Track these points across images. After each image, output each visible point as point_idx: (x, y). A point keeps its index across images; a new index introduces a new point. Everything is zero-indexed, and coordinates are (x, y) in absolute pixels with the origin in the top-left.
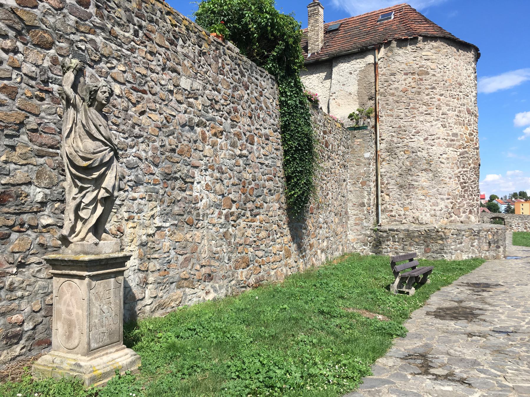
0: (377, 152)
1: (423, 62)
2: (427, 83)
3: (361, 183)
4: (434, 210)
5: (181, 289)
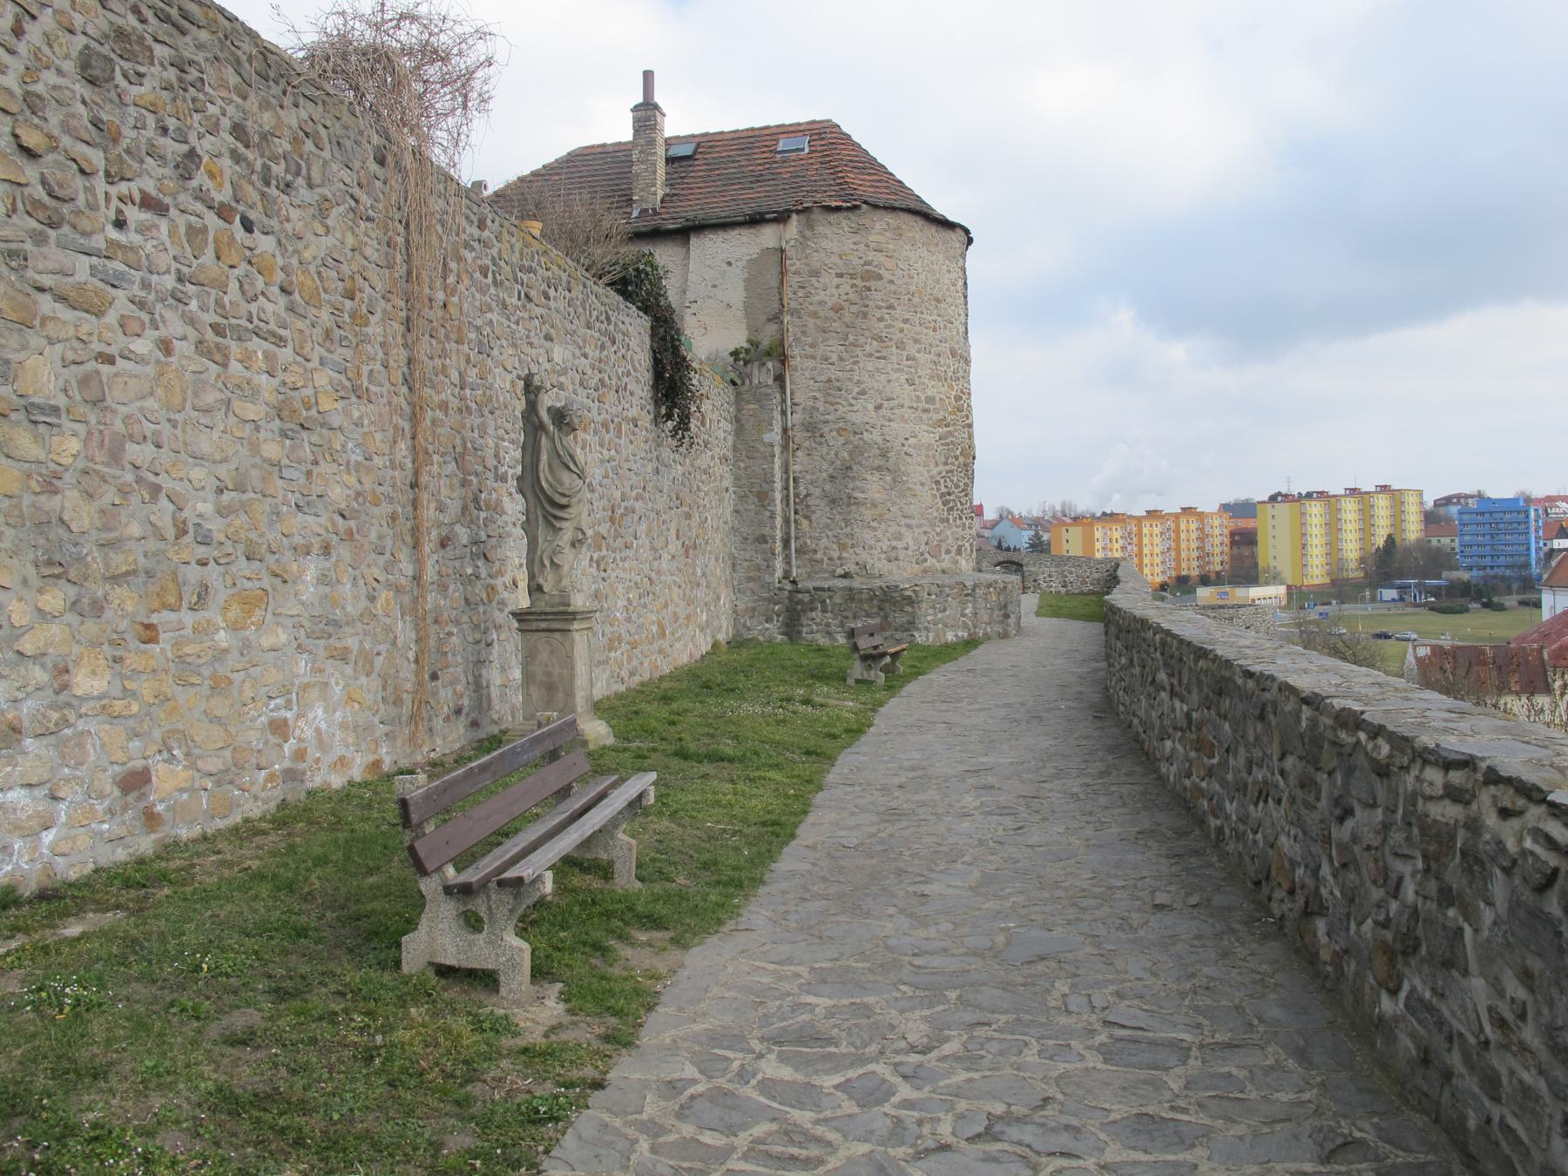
0: (785, 430)
1: (871, 255)
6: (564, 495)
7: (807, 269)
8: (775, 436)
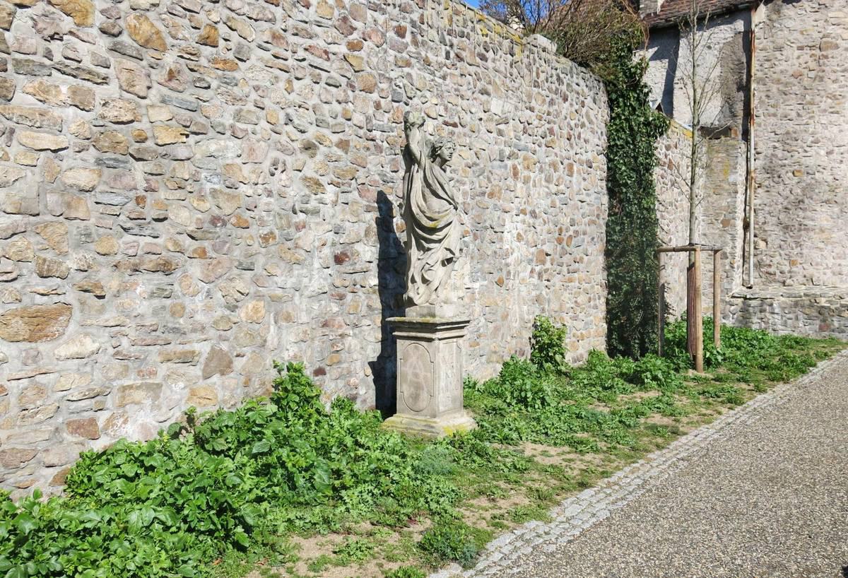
0: (748, 172)
1: (830, 29)
2: (835, 62)
3: (722, 222)
4: (839, 265)
5: (491, 365)
6: (431, 219)
7: (771, 45)
8: (740, 177)
